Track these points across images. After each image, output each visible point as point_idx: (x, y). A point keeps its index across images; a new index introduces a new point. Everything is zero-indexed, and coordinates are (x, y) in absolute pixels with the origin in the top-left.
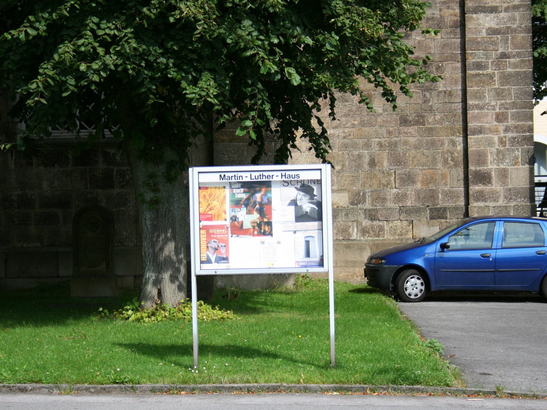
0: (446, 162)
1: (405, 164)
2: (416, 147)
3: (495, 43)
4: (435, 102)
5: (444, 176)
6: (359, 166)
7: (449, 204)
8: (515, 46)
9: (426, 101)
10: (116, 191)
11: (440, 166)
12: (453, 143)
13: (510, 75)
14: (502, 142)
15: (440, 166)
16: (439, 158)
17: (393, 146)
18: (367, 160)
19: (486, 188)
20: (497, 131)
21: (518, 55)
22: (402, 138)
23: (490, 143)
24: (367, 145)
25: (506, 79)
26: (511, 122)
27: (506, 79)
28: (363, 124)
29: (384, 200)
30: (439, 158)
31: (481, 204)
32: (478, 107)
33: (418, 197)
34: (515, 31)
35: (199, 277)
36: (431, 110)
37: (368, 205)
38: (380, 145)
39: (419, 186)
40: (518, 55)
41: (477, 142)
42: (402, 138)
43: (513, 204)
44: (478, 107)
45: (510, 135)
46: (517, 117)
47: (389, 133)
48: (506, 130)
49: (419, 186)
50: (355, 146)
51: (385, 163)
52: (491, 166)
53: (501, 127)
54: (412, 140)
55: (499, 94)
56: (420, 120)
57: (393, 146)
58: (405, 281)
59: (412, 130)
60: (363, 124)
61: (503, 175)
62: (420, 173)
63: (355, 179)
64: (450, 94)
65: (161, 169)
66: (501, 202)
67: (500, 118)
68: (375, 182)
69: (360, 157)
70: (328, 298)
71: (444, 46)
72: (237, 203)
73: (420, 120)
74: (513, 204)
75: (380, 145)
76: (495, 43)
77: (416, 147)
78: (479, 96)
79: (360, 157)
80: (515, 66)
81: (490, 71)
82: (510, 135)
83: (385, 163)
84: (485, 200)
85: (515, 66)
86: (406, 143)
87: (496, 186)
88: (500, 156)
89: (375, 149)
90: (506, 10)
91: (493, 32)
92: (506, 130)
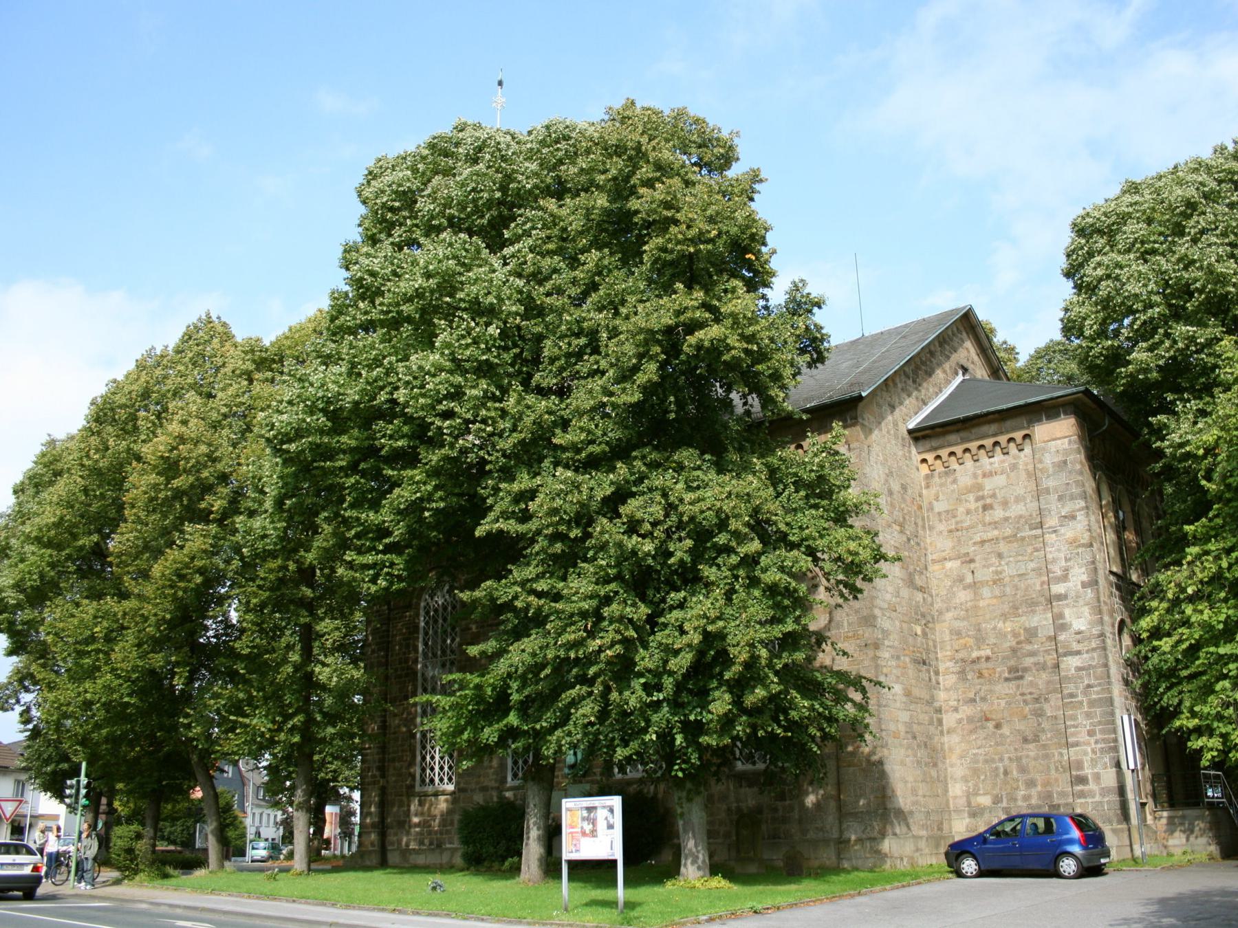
0: (1057, 769)
1: (1029, 773)
2: (1035, 759)
3: (1081, 678)
4: (1045, 725)
5: (1057, 780)
6: (997, 775)
7: (1062, 801)
8: (1096, 679)
9: (1039, 724)
10: (787, 802)
11: (1053, 772)
12: (1061, 754)
13: (1095, 700)
14: (1094, 752)
15: (1053, 772)
16: (1052, 766)
17: (1019, 759)
18: (1002, 770)
19: (1086, 788)
20: (1089, 744)
21: (1099, 684)
22: (1025, 753)
23: (1086, 754)
24: (1001, 760)
25: (1092, 703)
26: (1099, 736)
27: (1092, 703)
28: (997, 744)
29: (1016, 800)
30: (1052, 766)
31: (1083, 800)
32: (1074, 726)
33: (1039, 798)
34: (1094, 667)
35: (570, 862)
36: (1043, 730)
37: (1004, 804)
38: (1010, 759)
39: (1039, 788)
40: (1099, 684)
41: (1076, 753)
42: (1025, 753)
43: (1106, 799)
44: (1074, 726)
45: (1099, 746)
46: (1103, 732)
47: (1016, 749)
48: (1096, 742)
49: (1039, 788)
50: (993, 761)
51: (1015, 773)
52: (1088, 771)
53: (1092, 740)
54: (1032, 754)
55: (1088, 715)
56: (1036, 739)
57: (1019, 759)
58: (962, 862)
59: (1031, 746)
60: (997, 744)
61: (1097, 777)
62: (1039, 778)
63: (995, 785)
64: (1056, 717)
65: (684, 794)
66: (1098, 798)
67: (1091, 733)
68: (1008, 787)
69: (997, 768)
70: (569, 874)
71: (1049, 682)
72: (583, 819)
73: (1036, 739)
74: (1106, 799)
75: (1010, 759)
76: (1081, 678)
77: (1035, 759)
78: (1074, 718)
79: (997, 768)
80: (1098, 693)
81: (1080, 698)
82: (1099, 746)
83: (1015, 773)
84: (1085, 797)
85: (1098, 693)
86: (1027, 756)
87: (1092, 786)
88: (1094, 762)
89: (1006, 762)
90: (1087, 652)
91: (1079, 669)
92: (1096, 742)
